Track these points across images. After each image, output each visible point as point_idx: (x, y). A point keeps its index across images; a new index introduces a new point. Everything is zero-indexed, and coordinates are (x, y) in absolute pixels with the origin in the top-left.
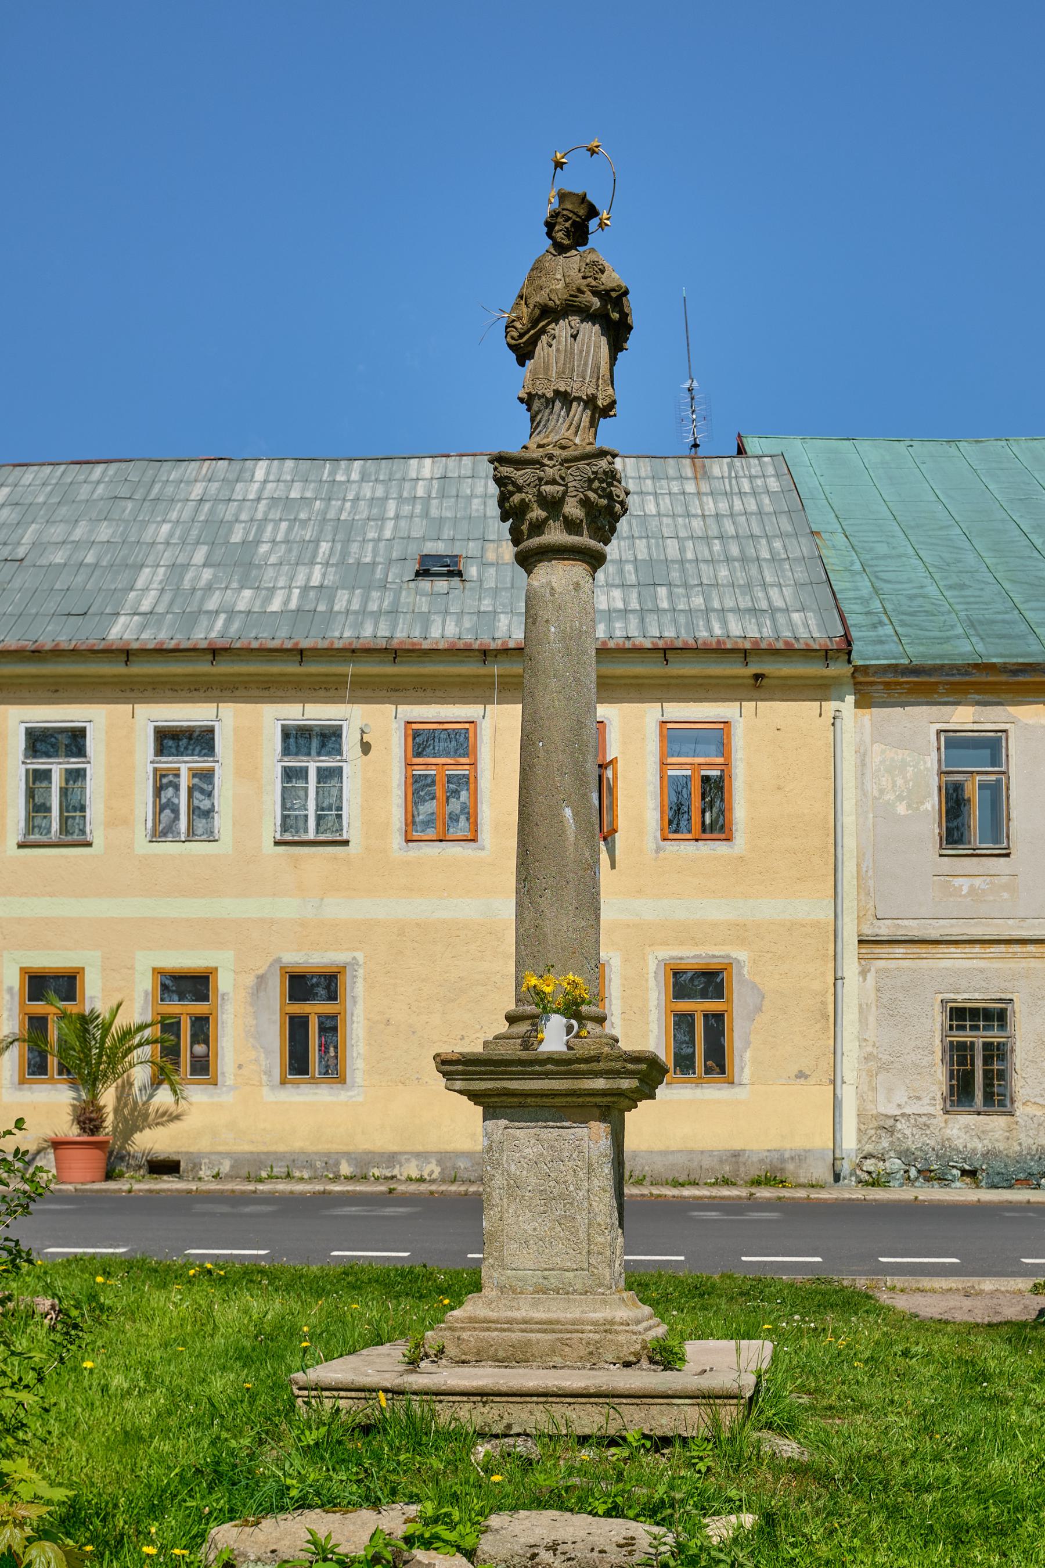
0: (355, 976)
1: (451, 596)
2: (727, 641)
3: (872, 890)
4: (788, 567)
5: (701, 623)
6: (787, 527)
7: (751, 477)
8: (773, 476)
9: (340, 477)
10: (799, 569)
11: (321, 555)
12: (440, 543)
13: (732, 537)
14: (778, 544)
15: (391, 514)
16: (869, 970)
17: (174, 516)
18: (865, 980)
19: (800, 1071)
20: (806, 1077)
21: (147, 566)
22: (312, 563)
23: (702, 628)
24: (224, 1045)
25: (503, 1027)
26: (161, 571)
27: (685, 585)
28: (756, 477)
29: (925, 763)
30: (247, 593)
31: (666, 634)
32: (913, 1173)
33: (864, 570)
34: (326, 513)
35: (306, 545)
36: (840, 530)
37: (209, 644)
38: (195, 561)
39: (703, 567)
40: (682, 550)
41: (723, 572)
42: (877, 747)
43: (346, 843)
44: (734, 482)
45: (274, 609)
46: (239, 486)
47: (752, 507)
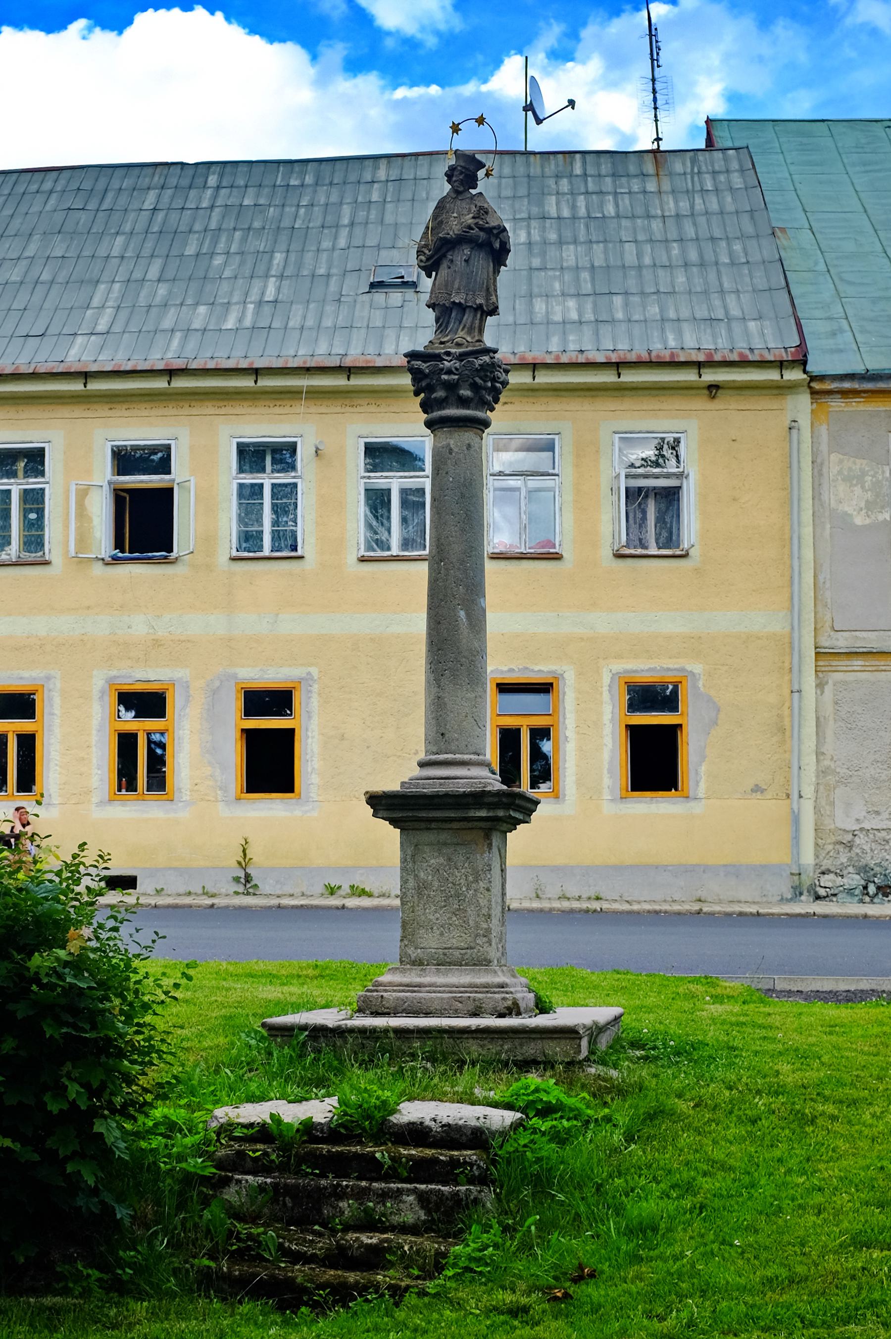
0: (310, 691)
1: (405, 309)
2: (681, 353)
3: (829, 601)
4: (747, 272)
5: (656, 334)
6: (749, 229)
7: (714, 173)
8: (736, 171)
9: (294, 182)
10: (759, 274)
11: (275, 267)
12: (395, 252)
13: (692, 240)
14: (737, 247)
15: (346, 221)
16: (827, 683)
17: (127, 228)
18: (822, 692)
19: (757, 785)
20: (763, 791)
21: (103, 283)
22: (267, 276)
23: (656, 340)
24: (180, 761)
25: (417, 772)
26: (117, 286)
27: (642, 293)
28: (719, 172)
29: (883, 472)
30: (202, 309)
31: (620, 347)
32: (872, 889)
33: (828, 271)
34: (280, 221)
35: (260, 255)
36: (807, 226)
37: (166, 365)
38: (149, 276)
39: (661, 272)
40: (639, 255)
41: (681, 279)
42: (834, 457)
43: (302, 557)
44: (696, 178)
45: (229, 327)
46: (193, 193)
47: (714, 206)
